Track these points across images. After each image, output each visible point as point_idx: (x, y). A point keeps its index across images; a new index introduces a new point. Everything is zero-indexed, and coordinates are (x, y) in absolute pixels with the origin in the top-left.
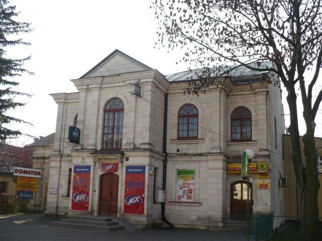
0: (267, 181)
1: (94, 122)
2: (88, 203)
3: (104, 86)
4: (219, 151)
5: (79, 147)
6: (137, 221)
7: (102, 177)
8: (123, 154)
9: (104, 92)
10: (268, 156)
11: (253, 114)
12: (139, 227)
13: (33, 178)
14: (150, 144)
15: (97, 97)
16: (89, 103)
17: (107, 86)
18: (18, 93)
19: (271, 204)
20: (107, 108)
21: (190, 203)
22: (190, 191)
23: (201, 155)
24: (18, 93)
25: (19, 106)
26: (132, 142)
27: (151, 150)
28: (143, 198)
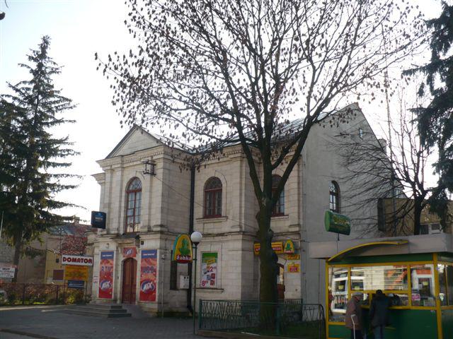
0: (298, 262)
1: (117, 204)
2: (111, 290)
3: (125, 166)
4: (238, 229)
5: (105, 232)
6: (150, 309)
7: (125, 262)
8: (138, 237)
9: (126, 172)
10: (297, 233)
11: (224, 185)
12: (151, 315)
13: (83, 266)
14: (299, 225)
15: (119, 178)
16: (114, 185)
17: (128, 165)
18: (68, 175)
19: (302, 290)
20: (131, 189)
21: (212, 289)
22: (213, 276)
23: (222, 235)
24: (68, 175)
25: (65, 190)
26: (147, 224)
27: (161, 232)
28: (155, 284)
